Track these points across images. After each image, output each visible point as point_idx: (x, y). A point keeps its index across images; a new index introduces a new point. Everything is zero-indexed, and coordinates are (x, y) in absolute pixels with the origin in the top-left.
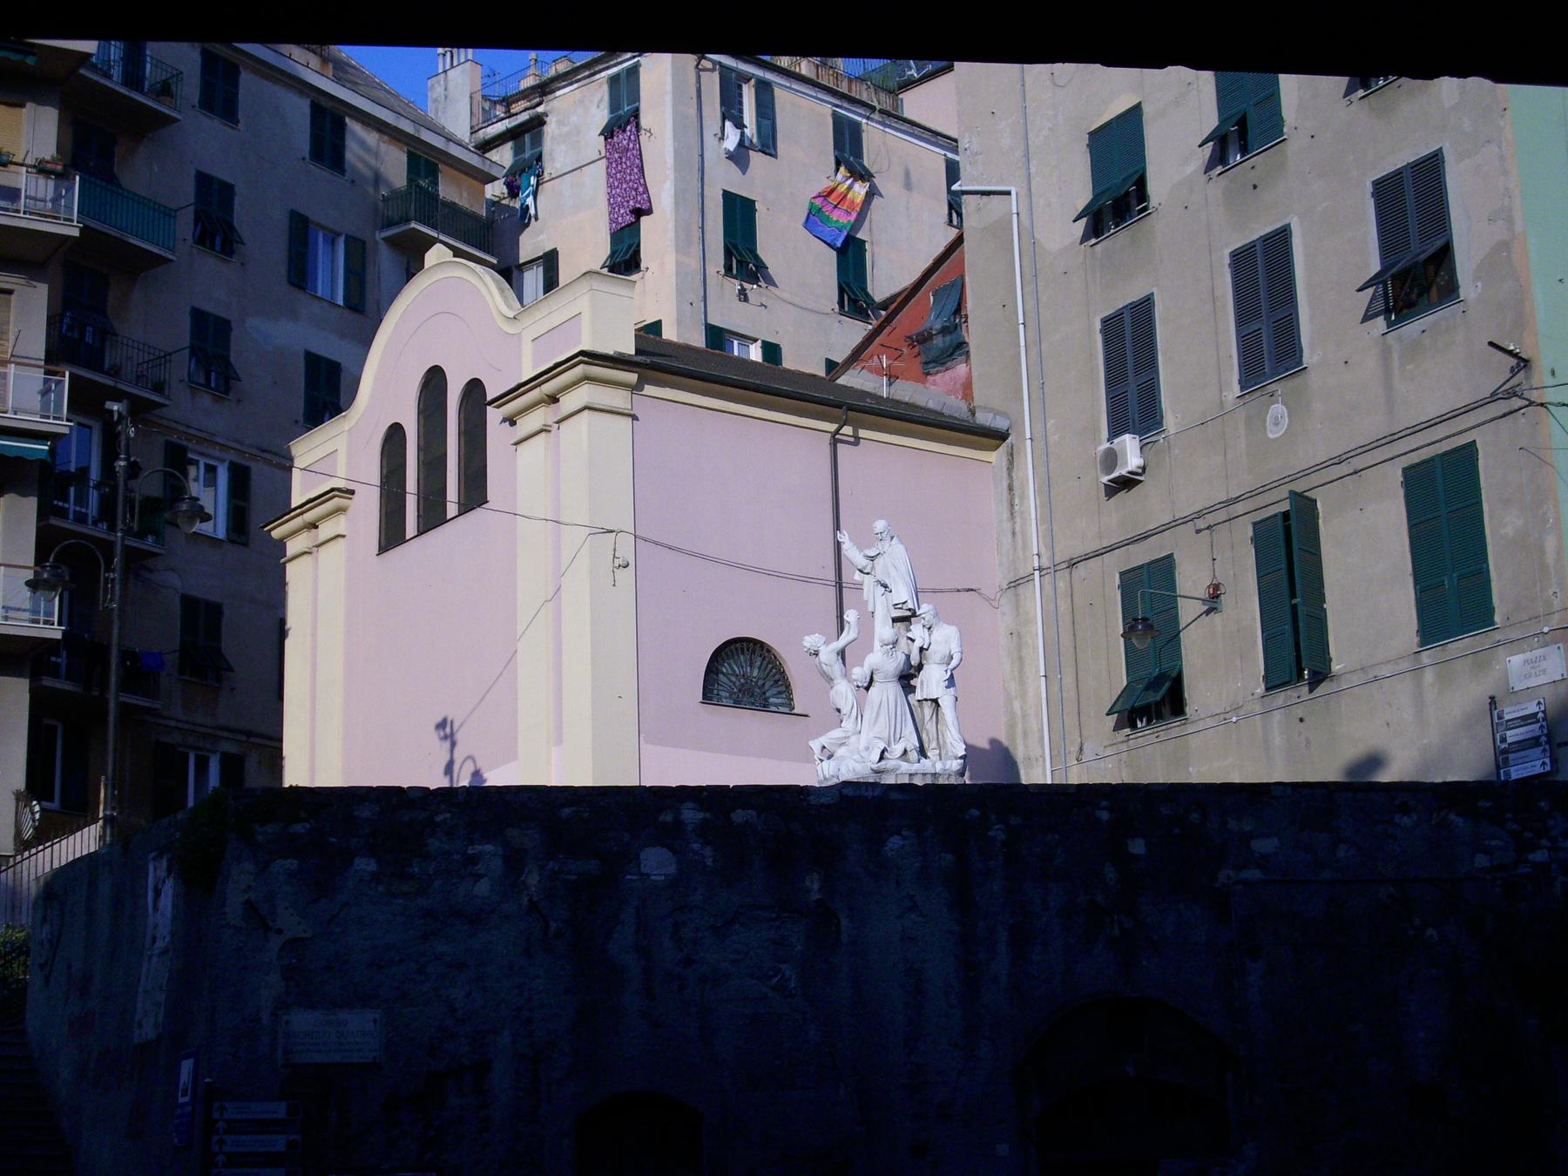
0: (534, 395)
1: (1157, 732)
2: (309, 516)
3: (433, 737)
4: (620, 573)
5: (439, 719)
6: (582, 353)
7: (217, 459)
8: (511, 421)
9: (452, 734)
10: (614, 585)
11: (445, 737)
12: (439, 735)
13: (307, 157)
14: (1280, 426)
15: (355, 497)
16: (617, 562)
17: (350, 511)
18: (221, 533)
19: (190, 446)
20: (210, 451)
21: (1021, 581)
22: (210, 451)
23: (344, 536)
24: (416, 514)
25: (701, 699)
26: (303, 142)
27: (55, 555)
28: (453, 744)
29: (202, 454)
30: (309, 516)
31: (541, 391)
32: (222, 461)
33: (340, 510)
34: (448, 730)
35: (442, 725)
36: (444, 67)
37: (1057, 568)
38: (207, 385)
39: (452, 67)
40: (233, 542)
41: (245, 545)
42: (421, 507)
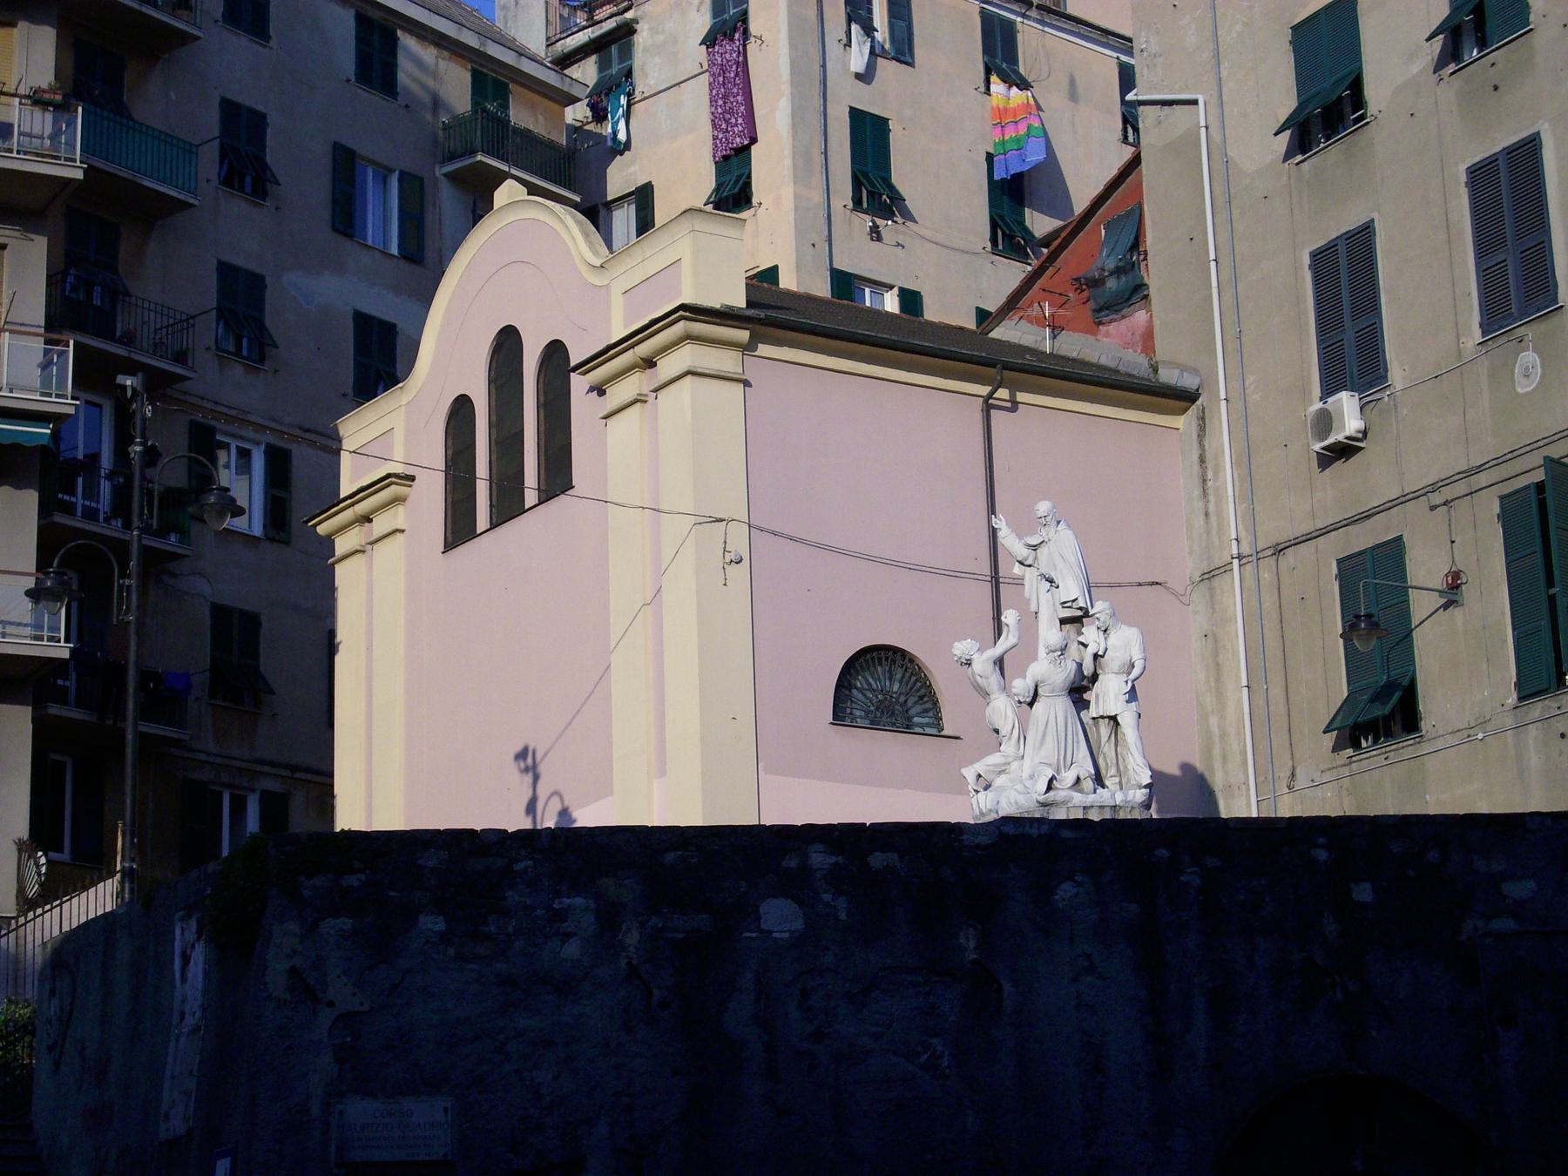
1: (1386, 752)
2: (362, 508)
4: (733, 570)
5: (519, 748)
6: (683, 307)
9: (535, 766)
10: (725, 585)
11: (527, 770)
12: (519, 765)
14: (1532, 377)
18: (258, 530)
21: (1216, 572)
26: (346, 59)
28: (536, 778)
29: (233, 436)
30: (362, 508)
31: (634, 353)
32: (258, 444)
33: (398, 500)
34: (530, 760)
35: (522, 755)
37: (1260, 555)
38: (238, 353)
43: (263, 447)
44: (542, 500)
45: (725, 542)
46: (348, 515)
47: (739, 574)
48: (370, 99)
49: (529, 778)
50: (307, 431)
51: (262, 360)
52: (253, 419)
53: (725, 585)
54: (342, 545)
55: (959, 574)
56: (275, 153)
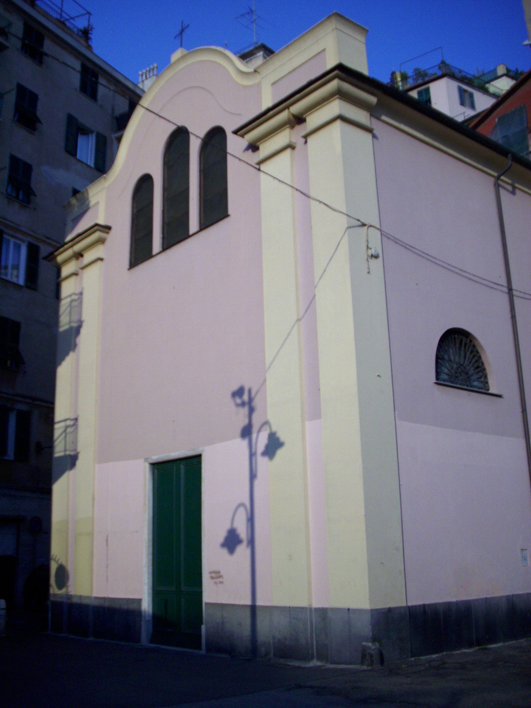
0: (284, 116)
2: (77, 248)
3: (229, 402)
4: (373, 262)
5: (235, 387)
6: (340, 67)
7: (21, 240)
8: (253, 147)
9: (251, 400)
10: (369, 272)
11: (243, 404)
12: (235, 401)
13: (78, 89)
15: (112, 232)
16: (370, 252)
17: (108, 242)
18: (21, 281)
19: (6, 230)
20: (18, 235)
22: (18, 235)
23: (101, 259)
24: (161, 235)
25: (434, 380)
26: (76, 79)
27: (320, 667)
28: (252, 410)
29: (12, 236)
30: (77, 248)
31: (289, 112)
32: (24, 241)
33: (101, 241)
34: (246, 397)
35: (239, 393)
36: (142, 79)
38: (17, 197)
39: (146, 78)
40: (27, 287)
41: (35, 289)
42: (165, 232)
43: (26, 243)
44: (202, 227)
45: (367, 241)
46: (69, 253)
47: (376, 265)
48: (85, 100)
49: (245, 411)
50: (49, 239)
51: (28, 202)
52: (22, 229)
53: (369, 272)
54: (65, 271)
55: (492, 285)
56: (41, 111)
